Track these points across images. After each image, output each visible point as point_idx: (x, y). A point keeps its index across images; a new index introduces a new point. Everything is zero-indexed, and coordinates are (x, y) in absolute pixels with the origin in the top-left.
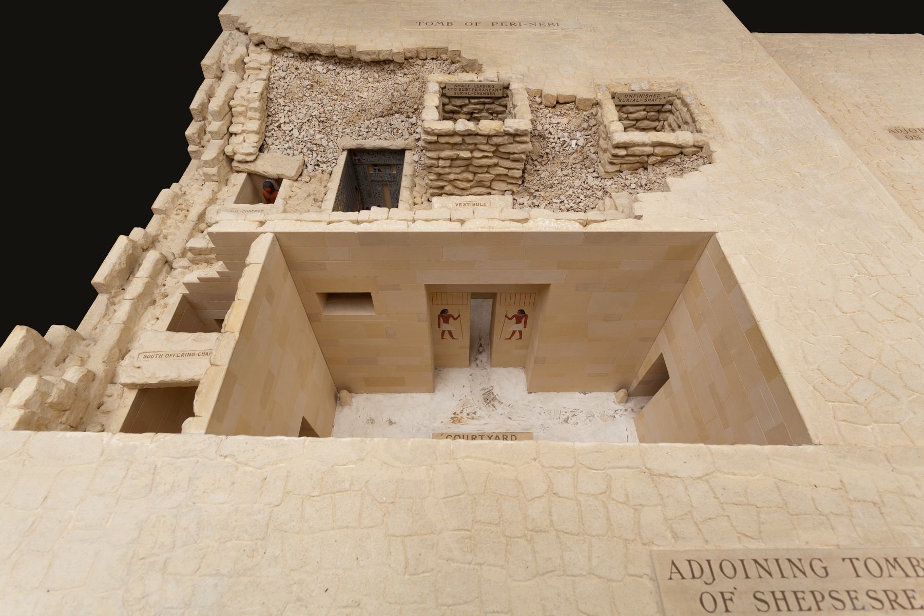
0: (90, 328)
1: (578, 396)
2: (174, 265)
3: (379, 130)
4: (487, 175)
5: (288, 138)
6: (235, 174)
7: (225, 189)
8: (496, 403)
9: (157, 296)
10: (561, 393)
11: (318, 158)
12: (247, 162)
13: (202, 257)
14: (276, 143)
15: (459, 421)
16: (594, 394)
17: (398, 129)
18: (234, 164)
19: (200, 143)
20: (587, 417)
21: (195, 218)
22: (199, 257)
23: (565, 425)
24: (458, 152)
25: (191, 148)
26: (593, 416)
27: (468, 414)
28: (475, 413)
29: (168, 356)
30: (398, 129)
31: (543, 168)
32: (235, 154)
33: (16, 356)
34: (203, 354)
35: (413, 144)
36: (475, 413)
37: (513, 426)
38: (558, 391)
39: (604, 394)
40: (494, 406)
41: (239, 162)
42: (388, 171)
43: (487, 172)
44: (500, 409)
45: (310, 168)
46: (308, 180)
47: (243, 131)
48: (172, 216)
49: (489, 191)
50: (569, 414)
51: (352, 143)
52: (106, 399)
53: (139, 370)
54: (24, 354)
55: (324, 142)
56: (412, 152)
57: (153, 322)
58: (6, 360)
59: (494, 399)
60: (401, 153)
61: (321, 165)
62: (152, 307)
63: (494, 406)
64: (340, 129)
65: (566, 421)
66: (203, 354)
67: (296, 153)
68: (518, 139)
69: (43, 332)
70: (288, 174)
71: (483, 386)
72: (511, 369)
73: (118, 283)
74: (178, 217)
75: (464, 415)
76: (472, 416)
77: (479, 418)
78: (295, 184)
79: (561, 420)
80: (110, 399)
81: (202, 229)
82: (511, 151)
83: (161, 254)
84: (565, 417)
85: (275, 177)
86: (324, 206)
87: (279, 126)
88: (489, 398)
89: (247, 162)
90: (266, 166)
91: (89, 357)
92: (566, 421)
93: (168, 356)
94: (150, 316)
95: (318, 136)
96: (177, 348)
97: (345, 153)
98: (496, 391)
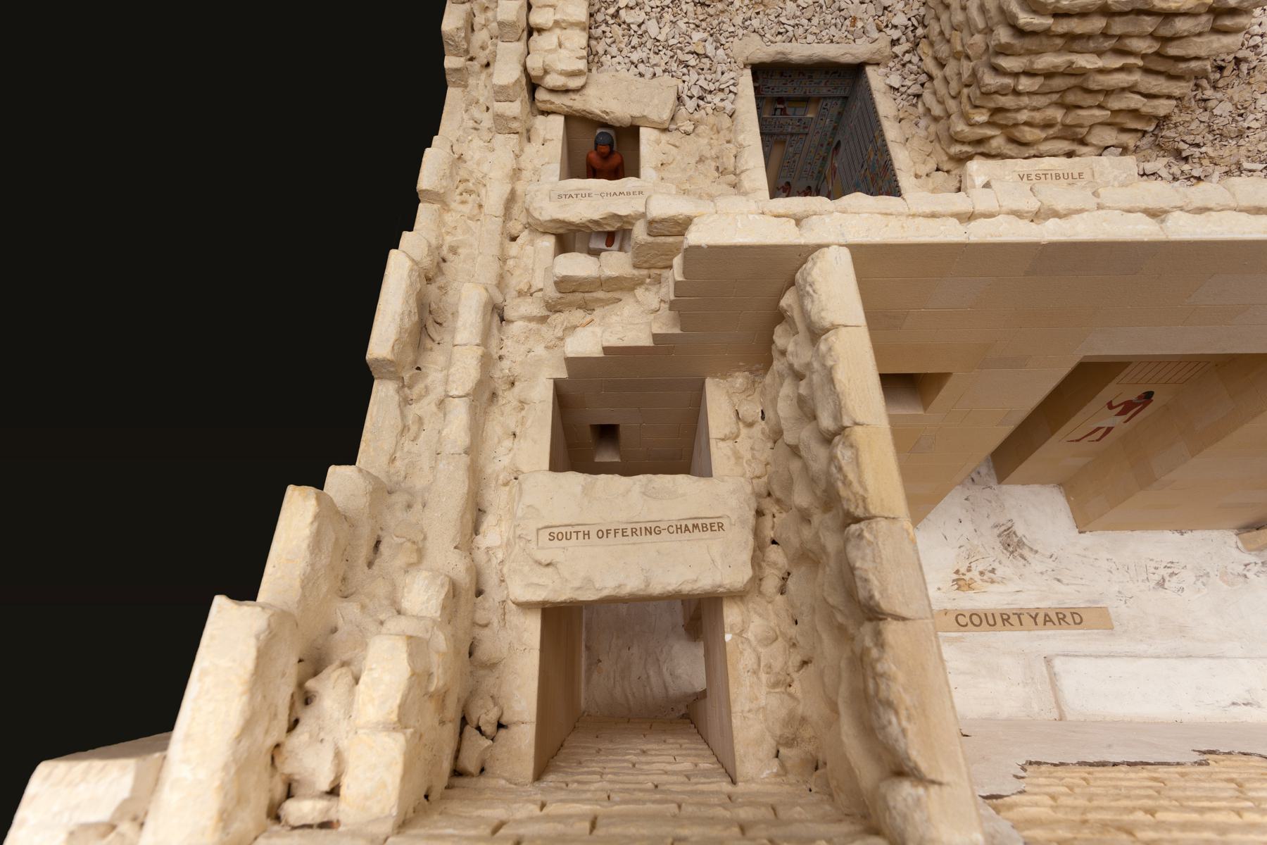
0: (384, 460)
1: (1171, 536)
2: (509, 314)
3: (815, 21)
4: (1097, 112)
5: (635, 41)
6: (541, 118)
7: (530, 149)
8: (1026, 552)
9: (501, 386)
10: (1137, 533)
11: (702, 83)
12: (567, 91)
13: (579, 296)
14: (614, 50)
15: (969, 587)
16: (1198, 534)
17: (855, 19)
18: (541, 95)
19: (467, 51)
20: (1198, 577)
21: (500, 210)
22: (570, 297)
23: (1161, 592)
24: (1074, 57)
25: (450, 62)
26: (1208, 575)
27: (982, 573)
28: (993, 571)
29: (602, 534)
30: (855, 19)
31: (1219, 95)
32: (546, 72)
33: (313, 565)
34: (679, 528)
35: (887, 51)
36: (993, 571)
37: (1067, 596)
38: (1147, 529)
39: (1215, 534)
40: (1022, 557)
41: (553, 91)
42: (800, 112)
43: (1100, 107)
44: (1037, 564)
45: (691, 104)
46: (690, 128)
47: (557, 23)
48: (454, 205)
49: (1075, 147)
50: (1165, 572)
51: (764, 51)
52: (478, 632)
53: (550, 569)
54: (324, 560)
55: (710, 49)
56: (882, 70)
57: (508, 443)
58: (297, 583)
59: (1020, 544)
60: (856, 71)
61: (709, 97)
62: (495, 409)
63: (1022, 557)
64: (738, 20)
65: (1161, 584)
66: (679, 528)
67: (659, 71)
68: (1228, 22)
69: (319, 484)
70: (654, 116)
71: (993, 520)
72: (1036, 488)
73: (410, 357)
74: (466, 209)
75: (975, 574)
76: (990, 575)
77: (1003, 580)
78: (665, 137)
79: (1152, 584)
80: (486, 632)
81: (514, 232)
82: (1192, 52)
83: (835, 327)
84: (1157, 577)
85: (627, 121)
86: (746, 183)
87: (615, 15)
88: (1011, 543)
89: (567, 91)
90: (609, 97)
91: (425, 538)
92: (1161, 584)
93: (602, 534)
94: (498, 430)
95: (697, 36)
96: (619, 516)
97: (748, 72)
98: (1020, 529)
